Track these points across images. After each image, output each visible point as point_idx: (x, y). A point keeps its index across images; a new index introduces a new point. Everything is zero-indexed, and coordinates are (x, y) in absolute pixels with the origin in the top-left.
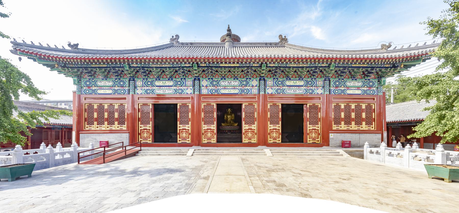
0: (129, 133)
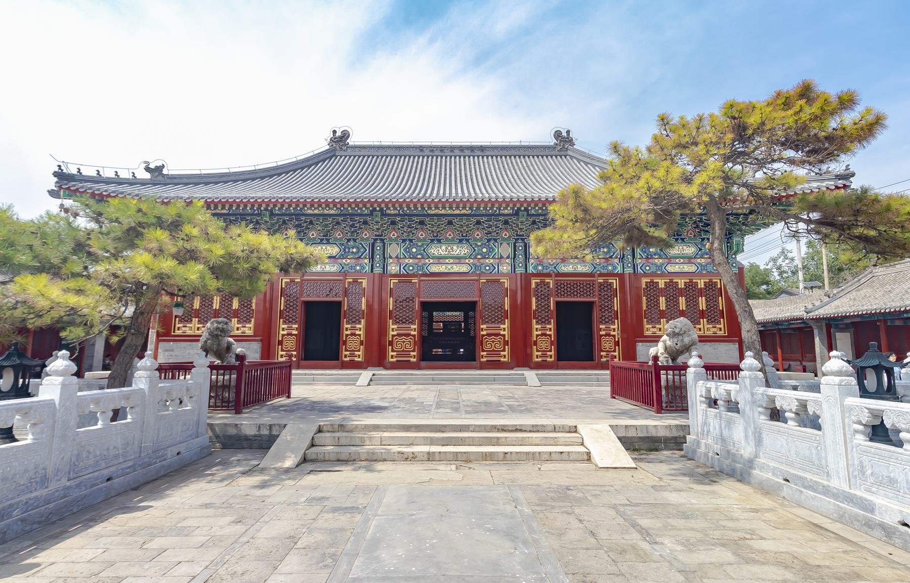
0: (261, 340)
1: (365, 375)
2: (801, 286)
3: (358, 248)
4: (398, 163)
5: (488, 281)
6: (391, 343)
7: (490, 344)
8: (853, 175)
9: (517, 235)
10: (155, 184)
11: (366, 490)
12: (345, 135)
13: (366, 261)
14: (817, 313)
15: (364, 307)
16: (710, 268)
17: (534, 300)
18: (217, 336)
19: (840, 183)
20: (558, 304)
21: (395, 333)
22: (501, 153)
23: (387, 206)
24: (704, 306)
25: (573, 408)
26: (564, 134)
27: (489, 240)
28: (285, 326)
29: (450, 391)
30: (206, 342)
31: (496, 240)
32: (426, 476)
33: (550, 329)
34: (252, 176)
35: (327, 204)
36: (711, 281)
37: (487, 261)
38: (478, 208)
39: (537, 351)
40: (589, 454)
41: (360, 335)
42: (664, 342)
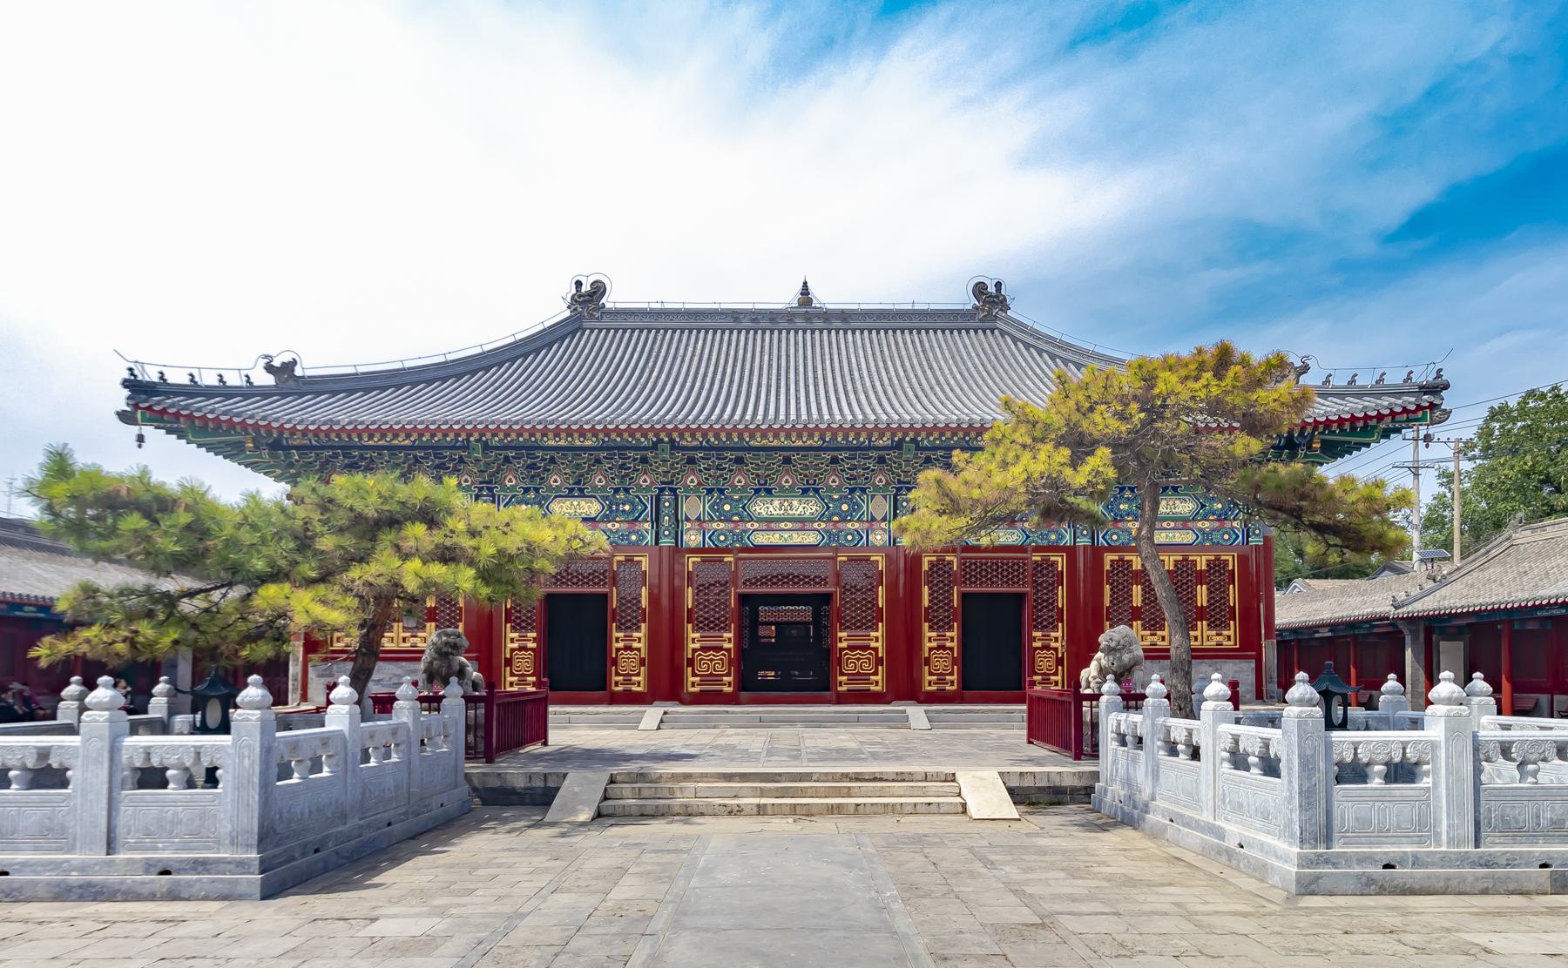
1: (652, 714)
2: (1416, 556)
3: (632, 504)
4: (697, 345)
5: (851, 559)
6: (691, 662)
7: (854, 663)
8: (1446, 386)
9: (900, 482)
10: (284, 396)
11: (686, 838)
12: (599, 289)
13: (647, 526)
14: (1410, 608)
15: (644, 603)
16: (1216, 537)
17: (926, 590)
18: (447, 654)
19: (1426, 399)
20: (964, 597)
21: (697, 645)
22: (878, 324)
23: (681, 436)
24: (1205, 599)
25: (962, 755)
26: (992, 289)
27: (852, 491)
28: (515, 635)
29: (786, 736)
30: (431, 663)
31: (863, 490)
32: (757, 827)
33: (952, 639)
34: (442, 373)
35: (582, 433)
36: (1218, 558)
37: (849, 525)
38: (834, 438)
39: (931, 674)
40: (964, 805)
41: (639, 650)
42: (1099, 660)
